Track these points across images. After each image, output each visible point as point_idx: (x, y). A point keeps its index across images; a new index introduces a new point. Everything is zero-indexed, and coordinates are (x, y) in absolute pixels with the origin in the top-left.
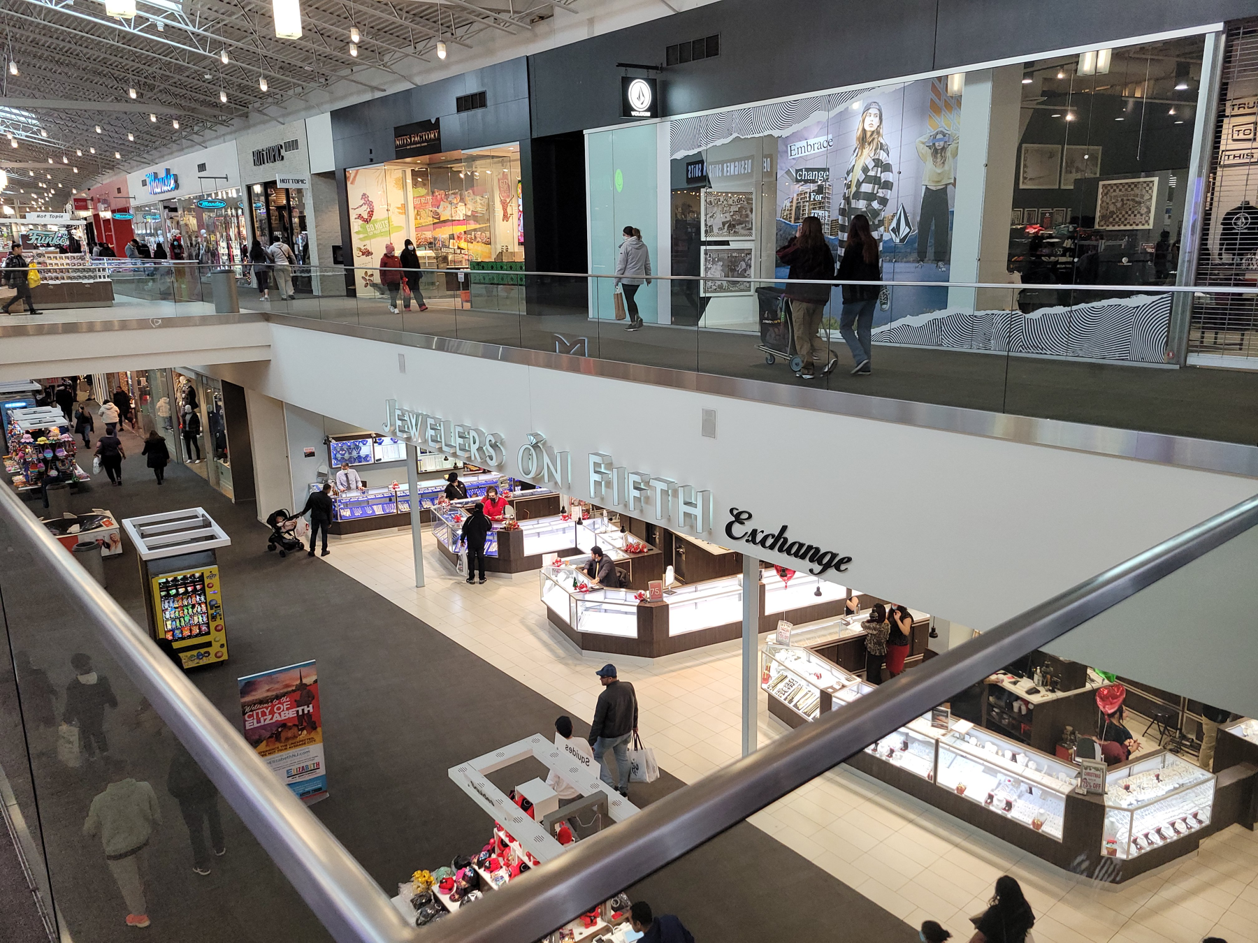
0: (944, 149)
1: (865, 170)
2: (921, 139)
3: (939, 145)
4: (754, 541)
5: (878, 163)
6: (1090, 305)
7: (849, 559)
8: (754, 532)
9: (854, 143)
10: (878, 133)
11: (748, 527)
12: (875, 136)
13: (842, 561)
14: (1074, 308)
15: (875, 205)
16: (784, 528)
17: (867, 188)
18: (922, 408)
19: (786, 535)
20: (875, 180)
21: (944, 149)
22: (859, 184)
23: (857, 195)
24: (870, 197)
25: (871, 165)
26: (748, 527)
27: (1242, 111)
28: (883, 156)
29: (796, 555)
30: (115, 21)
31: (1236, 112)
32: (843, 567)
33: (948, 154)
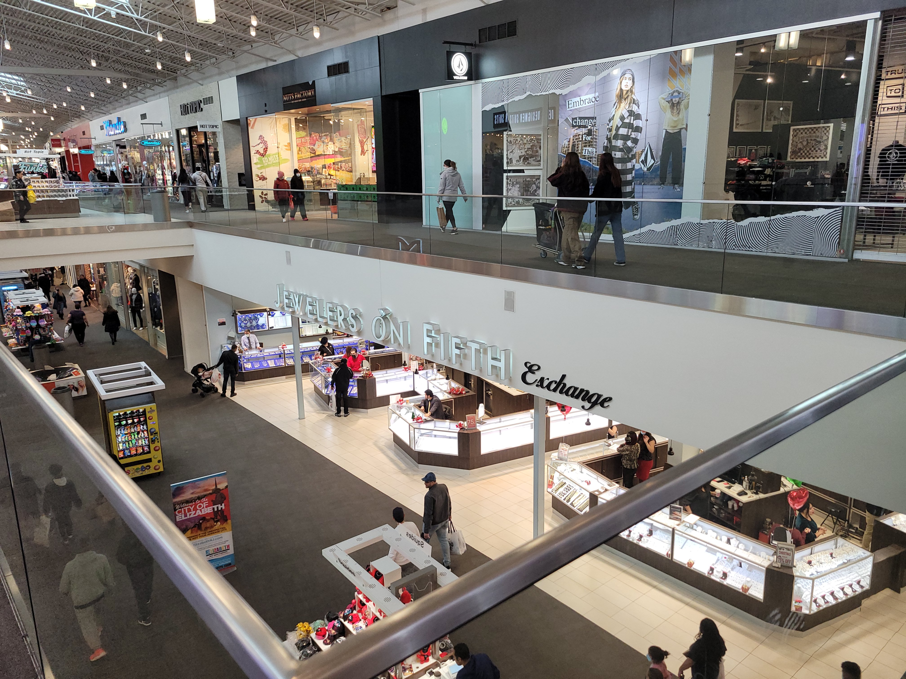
0: (679, 103)
1: (622, 118)
3: (675, 100)
4: (542, 386)
5: (631, 113)
7: (610, 399)
8: (542, 380)
9: (614, 99)
10: (632, 92)
11: (538, 376)
12: (629, 93)
13: (605, 400)
14: (772, 218)
15: (629, 143)
16: (564, 377)
19: (565, 381)
20: (629, 126)
21: (679, 103)
22: (618, 129)
23: (616, 137)
24: (626, 138)
27: (893, 76)
28: (635, 108)
29: (572, 396)
31: (889, 76)
32: (606, 404)
33: (682, 106)
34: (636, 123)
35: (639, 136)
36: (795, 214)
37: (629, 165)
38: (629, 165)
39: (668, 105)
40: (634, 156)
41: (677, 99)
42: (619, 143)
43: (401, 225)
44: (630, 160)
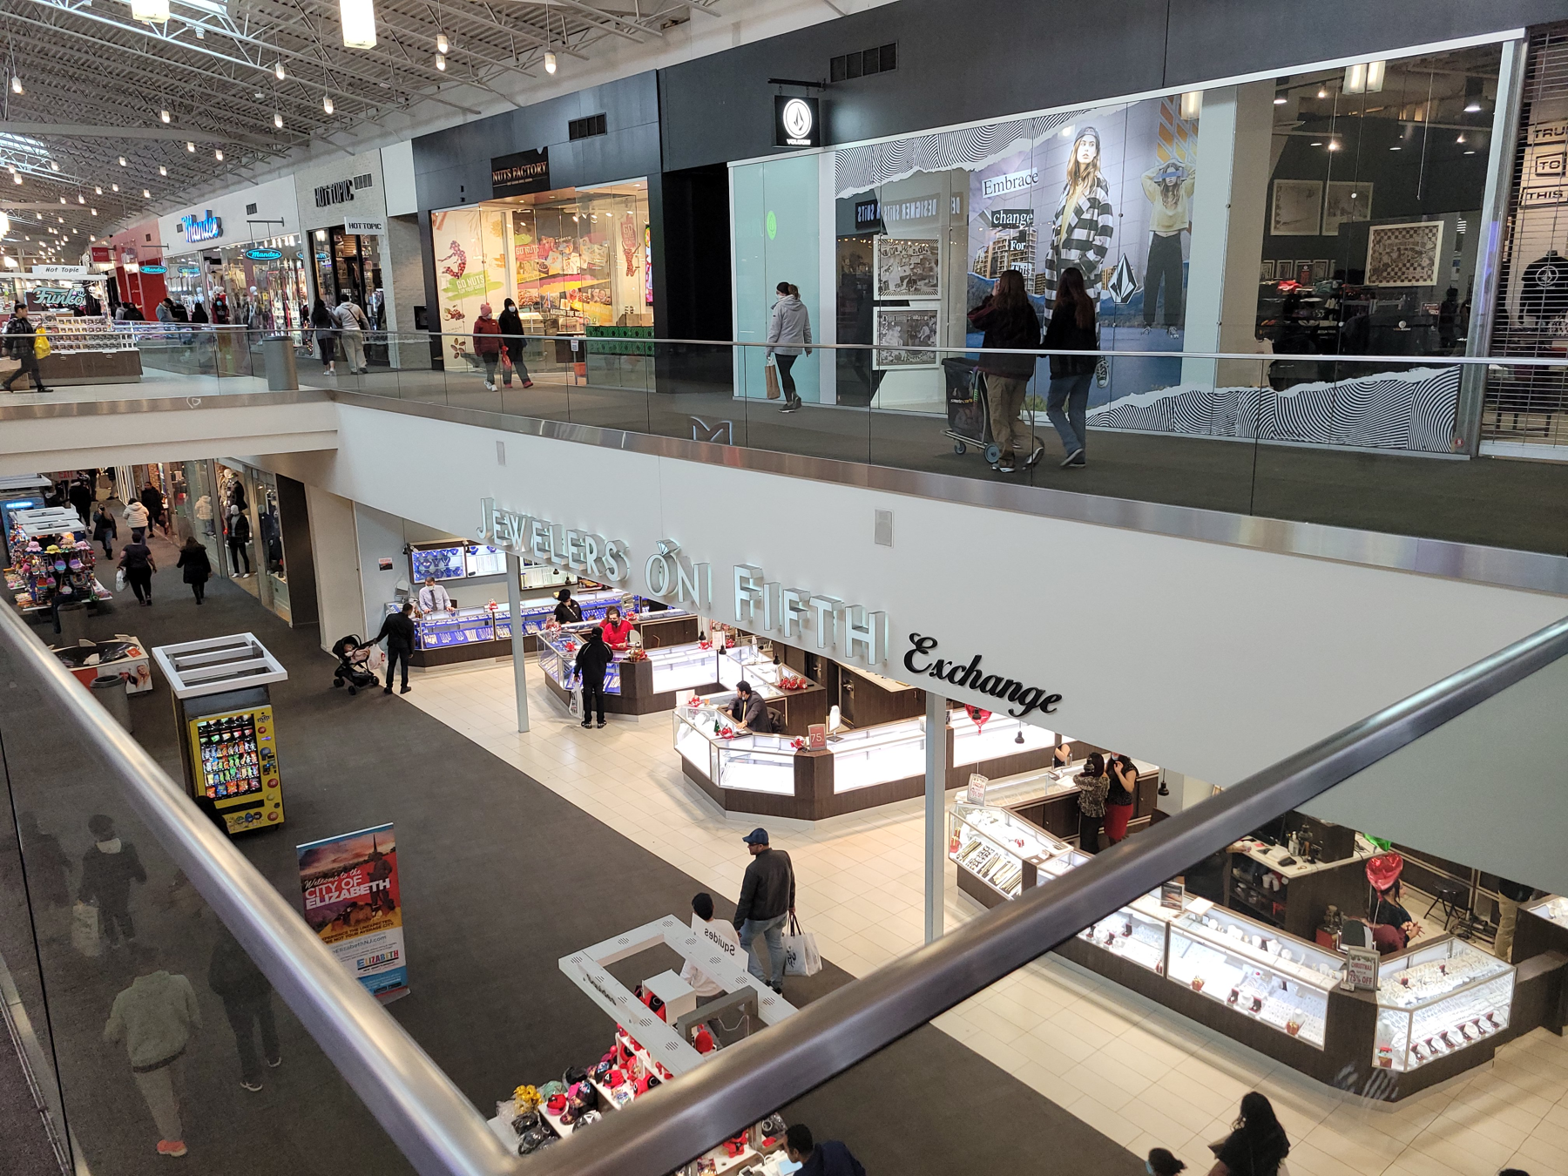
0: (1176, 185)
1: (1078, 211)
2: (1148, 173)
3: (1171, 180)
4: (939, 675)
5: (1094, 203)
6: (1358, 380)
7: (1059, 698)
8: (940, 664)
9: (1065, 178)
10: (1095, 166)
11: (933, 657)
12: (1091, 169)
13: (1049, 700)
14: (1339, 384)
15: (1091, 255)
16: (977, 659)
17: (1080, 234)
19: (980, 667)
20: (1091, 225)
21: (1176, 185)
22: (1071, 230)
23: (1069, 244)
24: (1085, 246)
25: (1086, 205)
27: (1548, 139)
28: (1100, 194)
29: (992, 692)
31: (1541, 139)
32: (1050, 707)
33: (1182, 192)
34: (1103, 220)
35: (1108, 242)
41: (1174, 179)
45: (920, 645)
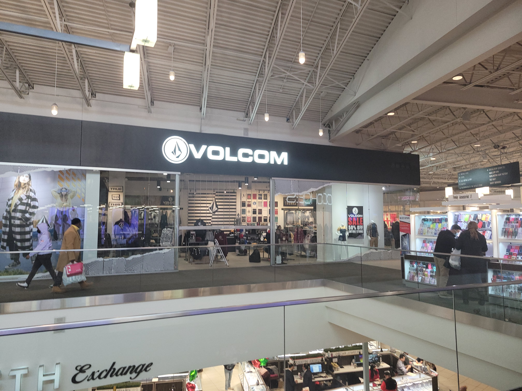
0: (66, 195)
1: (21, 199)
2: (54, 190)
3: (64, 193)
4: (93, 379)
5: (28, 197)
6: (149, 253)
7: (152, 364)
8: (93, 373)
9: (13, 187)
10: (29, 184)
11: (89, 373)
12: (27, 185)
13: (148, 366)
14: (144, 255)
15: (27, 215)
16: (114, 363)
17: (22, 208)
18: (300, 282)
19: (114, 367)
20: (28, 205)
21: (66, 195)
22: (16, 205)
23: (15, 210)
24: (24, 212)
25: (24, 198)
26: (89, 373)
27: (114, 190)
28: (32, 194)
29: (121, 374)
30: (439, 175)
31: (112, 190)
32: (148, 369)
33: (69, 197)
34: (32, 204)
35: (35, 210)
36: (154, 252)
37: (27, 229)
38: (27, 229)
39: (58, 195)
40: (31, 223)
41: (65, 193)
42: (19, 215)
43: (311, 286)
44: (28, 226)
45: (82, 370)
